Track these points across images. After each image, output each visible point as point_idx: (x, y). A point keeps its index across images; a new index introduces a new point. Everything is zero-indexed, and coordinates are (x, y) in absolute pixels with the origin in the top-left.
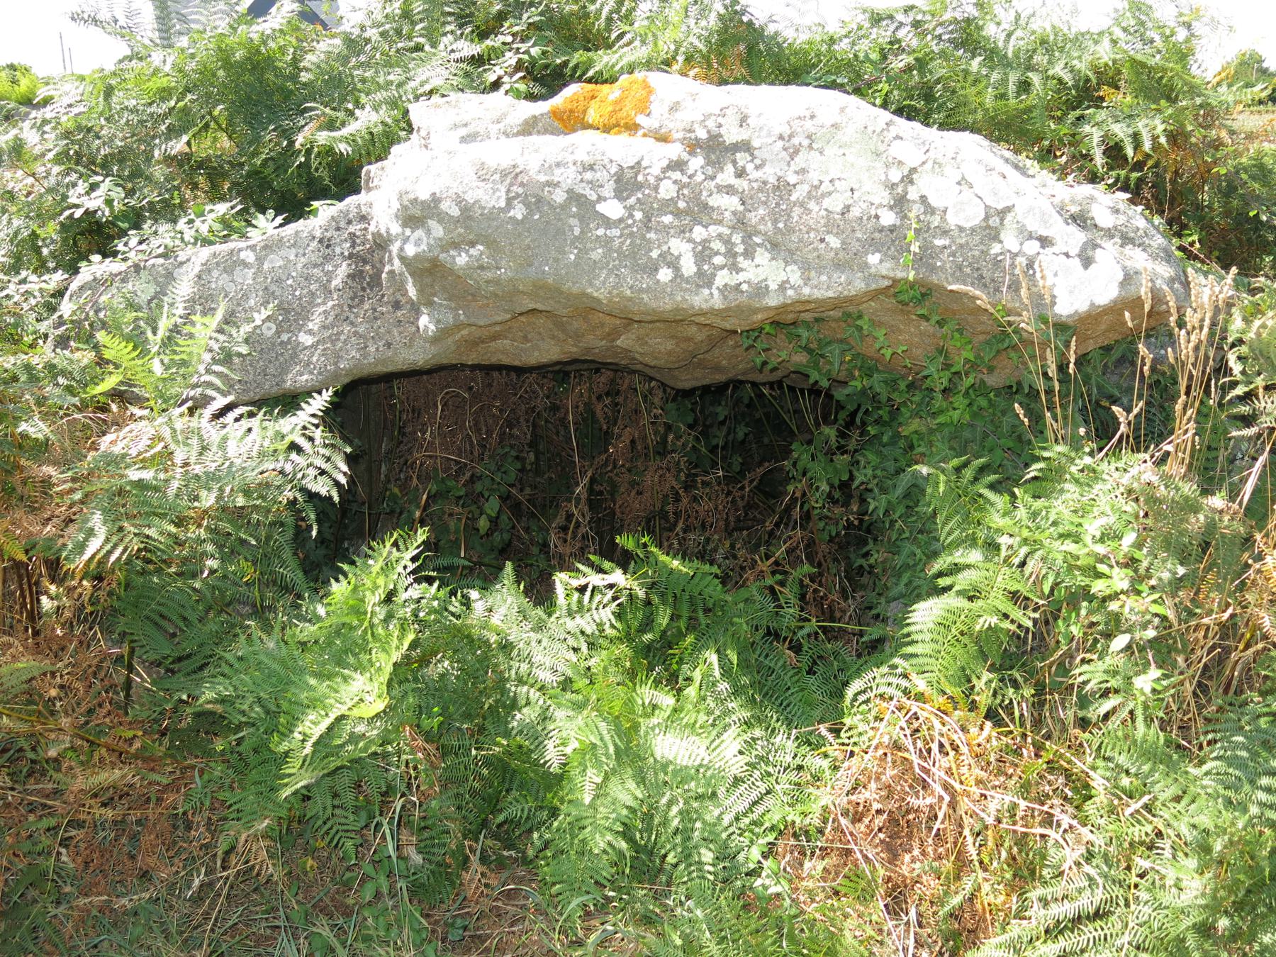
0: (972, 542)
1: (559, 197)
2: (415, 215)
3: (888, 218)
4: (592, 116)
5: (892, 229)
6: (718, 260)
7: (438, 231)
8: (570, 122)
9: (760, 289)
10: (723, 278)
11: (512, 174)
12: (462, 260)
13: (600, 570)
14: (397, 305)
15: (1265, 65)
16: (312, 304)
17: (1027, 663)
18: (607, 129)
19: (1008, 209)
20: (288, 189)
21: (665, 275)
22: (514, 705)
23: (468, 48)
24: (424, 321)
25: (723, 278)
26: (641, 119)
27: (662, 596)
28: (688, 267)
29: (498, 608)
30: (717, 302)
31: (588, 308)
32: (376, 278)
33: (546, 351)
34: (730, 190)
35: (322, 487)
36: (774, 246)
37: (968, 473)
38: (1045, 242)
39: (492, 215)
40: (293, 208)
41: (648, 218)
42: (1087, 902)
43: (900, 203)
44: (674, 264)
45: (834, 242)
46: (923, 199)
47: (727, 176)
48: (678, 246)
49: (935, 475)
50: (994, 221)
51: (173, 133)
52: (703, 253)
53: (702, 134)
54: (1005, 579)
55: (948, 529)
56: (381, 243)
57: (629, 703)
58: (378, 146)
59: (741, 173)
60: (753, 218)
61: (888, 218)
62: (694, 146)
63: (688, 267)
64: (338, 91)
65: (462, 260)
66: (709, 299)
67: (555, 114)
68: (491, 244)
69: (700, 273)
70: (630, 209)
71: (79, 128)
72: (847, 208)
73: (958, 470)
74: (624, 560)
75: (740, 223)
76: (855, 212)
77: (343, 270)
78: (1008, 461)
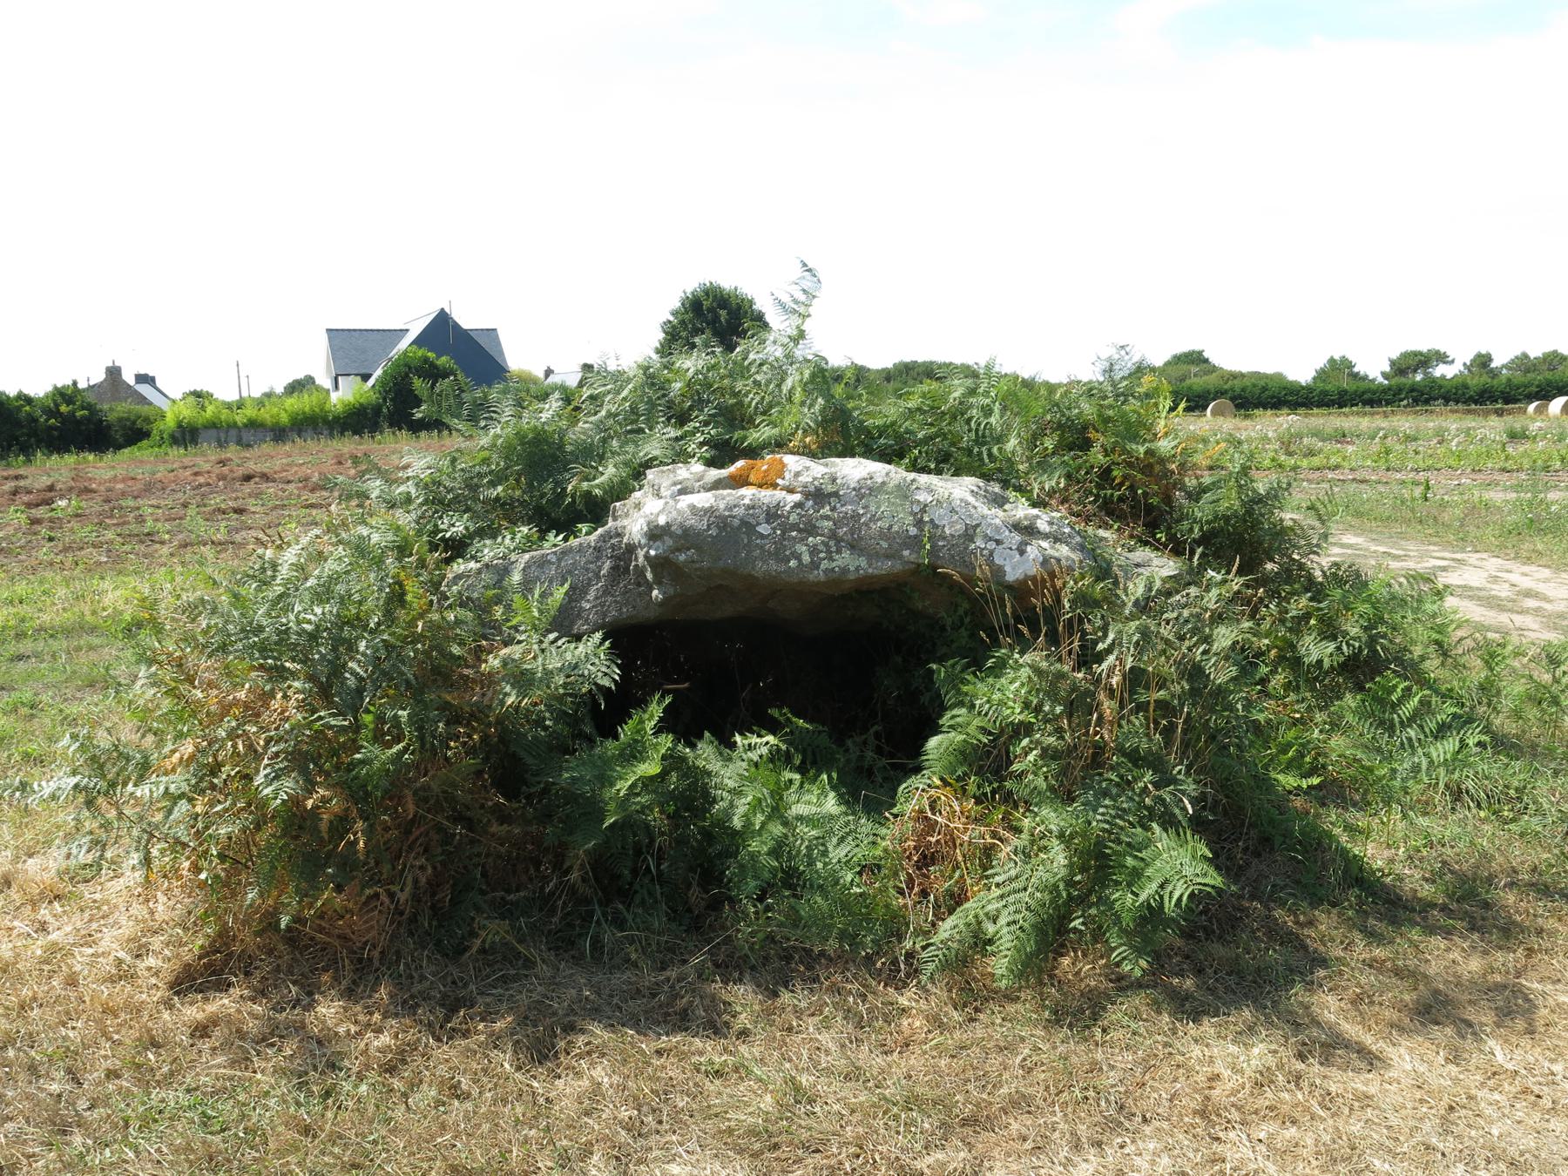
0: (961, 704)
1: (736, 522)
2: (655, 533)
3: (913, 531)
4: (752, 478)
5: (916, 537)
6: (822, 555)
7: (669, 542)
8: (739, 481)
9: (845, 570)
10: (825, 565)
11: (710, 511)
12: (682, 557)
13: (759, 736)
14: (639, 585)
15: (1356, 370)
16: (589, 585)
17: (989, 763)
18: (760, 486)
19: (978, 525)
20: (559, 516)
21: (793, 563)
22: (715, 801)
23: (673, 432)
24: (655, 592)
25: (825, 565)
26: (779, 481)
27: (796, 749)
28: (806, 558)
29: (705, 754)
30: (822, 577)
31: (751, 582)
32: (627, 570)
33: (728, 610)
34: (827, 518)
35: (606, 682)
36: (852, 547)
37: (959, 668)
38: (998, 542)
39: (699, 534)
40: (566, 526)
41: (783, 533)
42: (1013, 873)
43: (919, 523)
44: (798, 557)
45: (885, 545)
46: (932, 521)
47: (826, 510)
48: (801, 548)
49: (940, 671)
50: (971, 532)
51: (493, 484)
52: (814, 551)
53: (812, 489)
54: (977, 722)
55: (949, 699)
56: (631, 549)
57: (777, 783)
58: (620, 491)
59: (833, 509)
60: (841, 532)
61: (913, 531)
62: (807, 495)
63: (806, 558)
64: (592, 454)
65: (682, 557)
66: (819, 575)
67: (731, 477)
68: (699, 548)
69: (812, 562)
70: (774, 529)
71: (434, 483)
72: (891, 527)
73: (953, 666)
74: (774, 727)
75: (833, 535)
76: (896, 528)
77: (608, 564)
78: (977, 659)
